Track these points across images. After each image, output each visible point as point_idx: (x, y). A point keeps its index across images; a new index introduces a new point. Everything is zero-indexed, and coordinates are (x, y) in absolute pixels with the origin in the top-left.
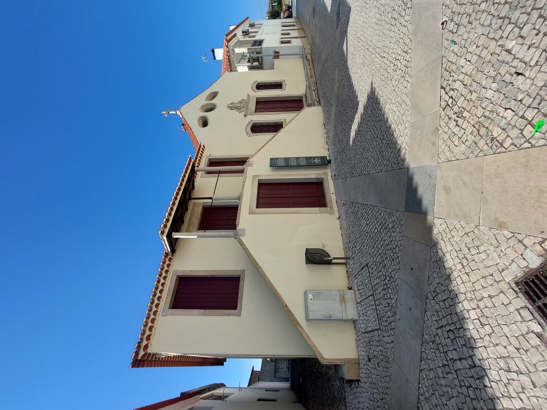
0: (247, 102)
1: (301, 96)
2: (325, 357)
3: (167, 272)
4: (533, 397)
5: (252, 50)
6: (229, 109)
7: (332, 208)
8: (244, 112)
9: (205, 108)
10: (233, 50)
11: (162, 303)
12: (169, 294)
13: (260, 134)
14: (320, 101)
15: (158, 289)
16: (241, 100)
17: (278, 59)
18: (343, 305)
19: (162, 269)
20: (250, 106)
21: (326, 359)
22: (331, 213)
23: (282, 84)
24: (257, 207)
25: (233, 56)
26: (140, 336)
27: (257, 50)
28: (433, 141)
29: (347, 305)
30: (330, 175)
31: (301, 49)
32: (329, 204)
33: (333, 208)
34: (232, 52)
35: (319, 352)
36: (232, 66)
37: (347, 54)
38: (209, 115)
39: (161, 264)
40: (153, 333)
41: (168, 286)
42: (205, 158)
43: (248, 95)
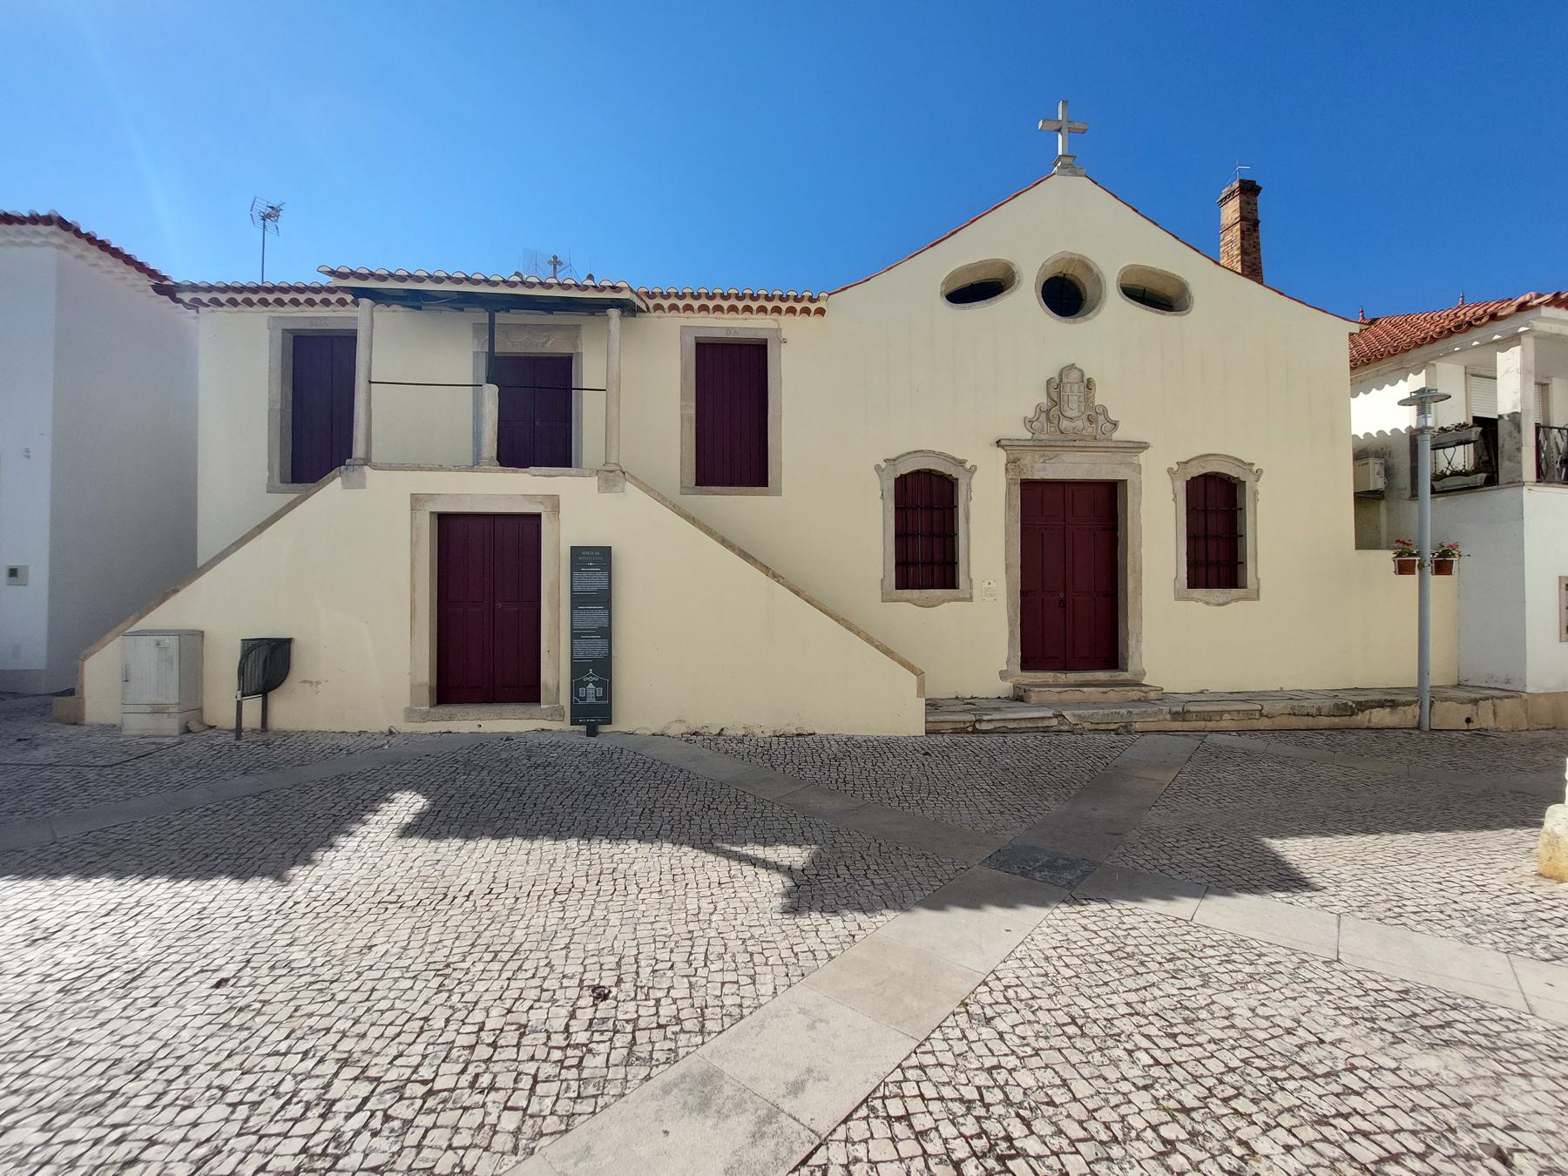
0: (1095, 444)
1: (1127, 664)
2: (87, 663)
3: (777, 310)
4: (1096, 1107)
5: (1510, 434)
6: (1055, 375)
7: (425, 718)
8: (1029, 436)
9: (1132, 281)
10: (1513, 339)
11: (290, 311)
12: (733, 331)
13: (892, 505)
14: (973, 732)
15: (707, 301)
16: (1113, 417)
17: (1392, 566)
18: (149, 709)
19: (796, 299)
20: (1068, 457)
21: (83, 665)
22: (410, 714)
23: (1237, 587)
24: (538, 516)
25: (1475, 343)
26: (733, 291)
27: (1509, 460)
28: (657, 1092)
29: (148, 716)
30: (554, 726)
31: (1508, 682)
32: (441, 711)
33: (425, 720)
34: (1496, 337)
35: (94, 652)
36: (1426, 350)
37: (754, 862)
38: (1115, 310)
39: (806, 294)
40: (726, 316)
41: (334, 315)
42: (773, 325)
43: (1142, 446)
